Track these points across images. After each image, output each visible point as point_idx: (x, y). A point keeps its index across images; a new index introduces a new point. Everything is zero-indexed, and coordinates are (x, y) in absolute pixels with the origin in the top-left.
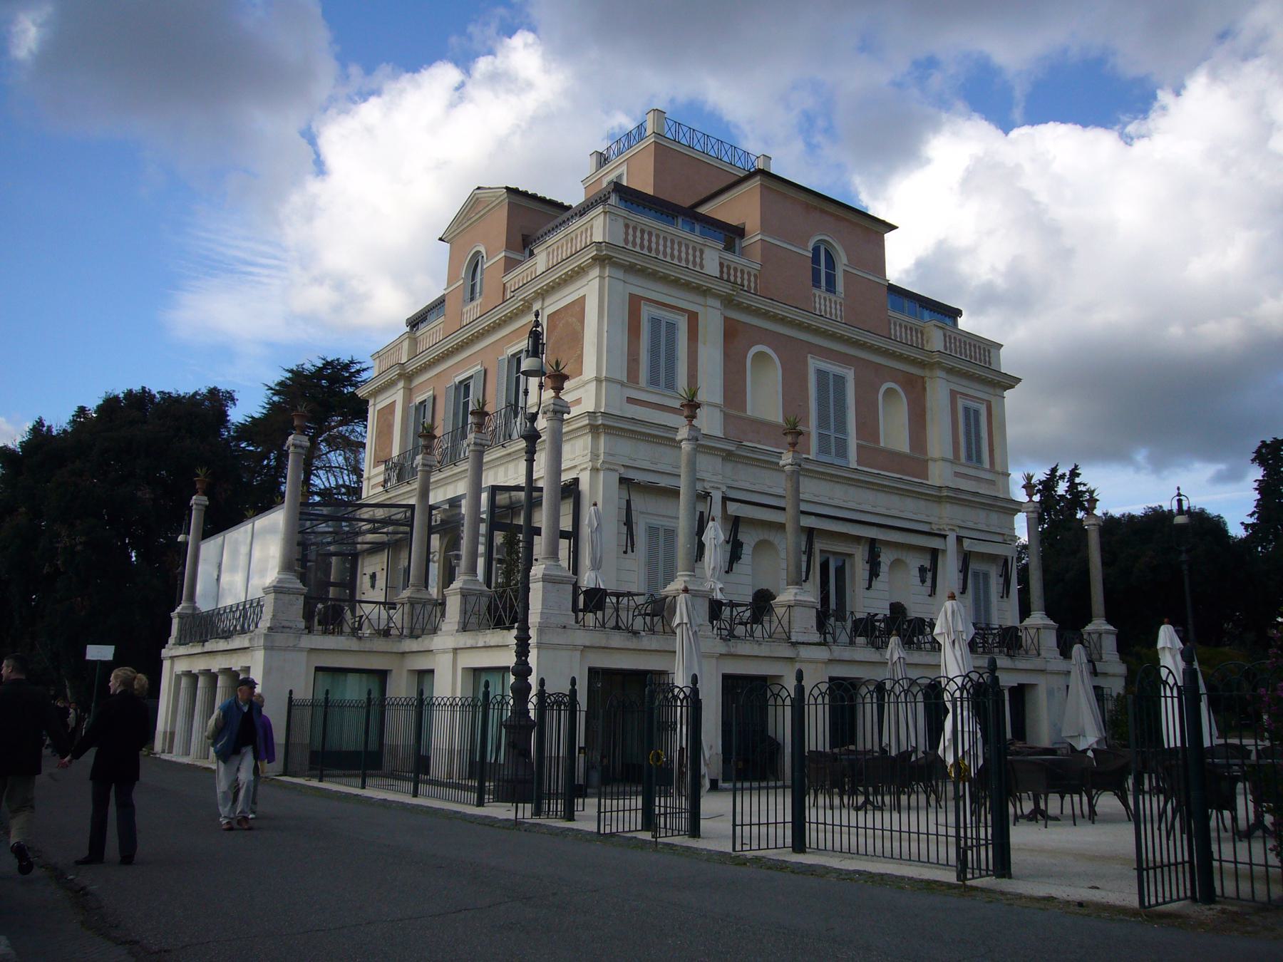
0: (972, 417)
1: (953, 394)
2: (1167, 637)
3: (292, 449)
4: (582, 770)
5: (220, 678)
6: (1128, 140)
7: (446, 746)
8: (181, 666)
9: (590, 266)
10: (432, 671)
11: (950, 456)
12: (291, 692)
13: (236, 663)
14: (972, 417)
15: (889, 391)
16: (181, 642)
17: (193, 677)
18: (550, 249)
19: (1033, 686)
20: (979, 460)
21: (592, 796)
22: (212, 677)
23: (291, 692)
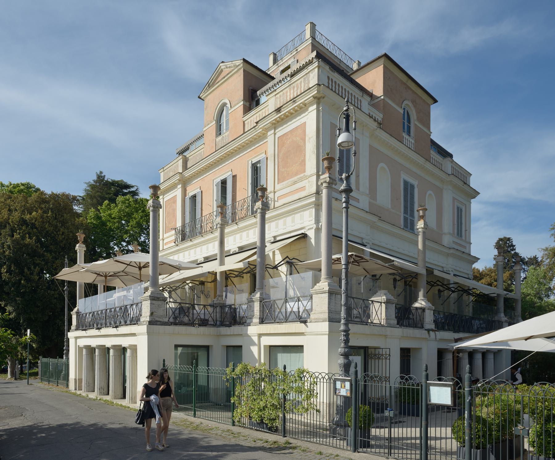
0: (459, 211)
1: (454, 199)
2: (29, 331)
3: (151, 209)
4: (466, 412)
5: (97, 350)
6: (100, 178)
7: (74, 378)
8: (82, 343)
9: (311, 104)
10: (241, 346)
11: (452, 232)
12: (164, 360)
13: (125, 342)
14: (459, 211)
15: (430, 194)
16: (77, 329)
17: (91, 350)
18: (278, 96)
19: (418, 350)
20: (461, 236)
21: (438, 427)
22: (106, 350)
23: (164, 360)
